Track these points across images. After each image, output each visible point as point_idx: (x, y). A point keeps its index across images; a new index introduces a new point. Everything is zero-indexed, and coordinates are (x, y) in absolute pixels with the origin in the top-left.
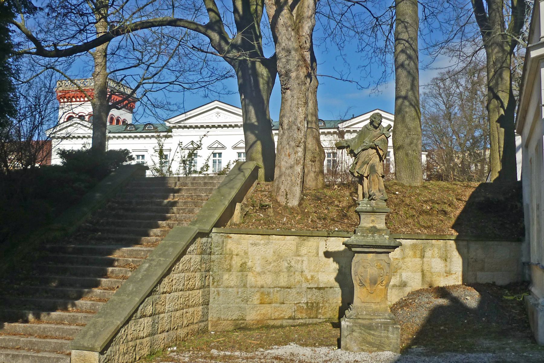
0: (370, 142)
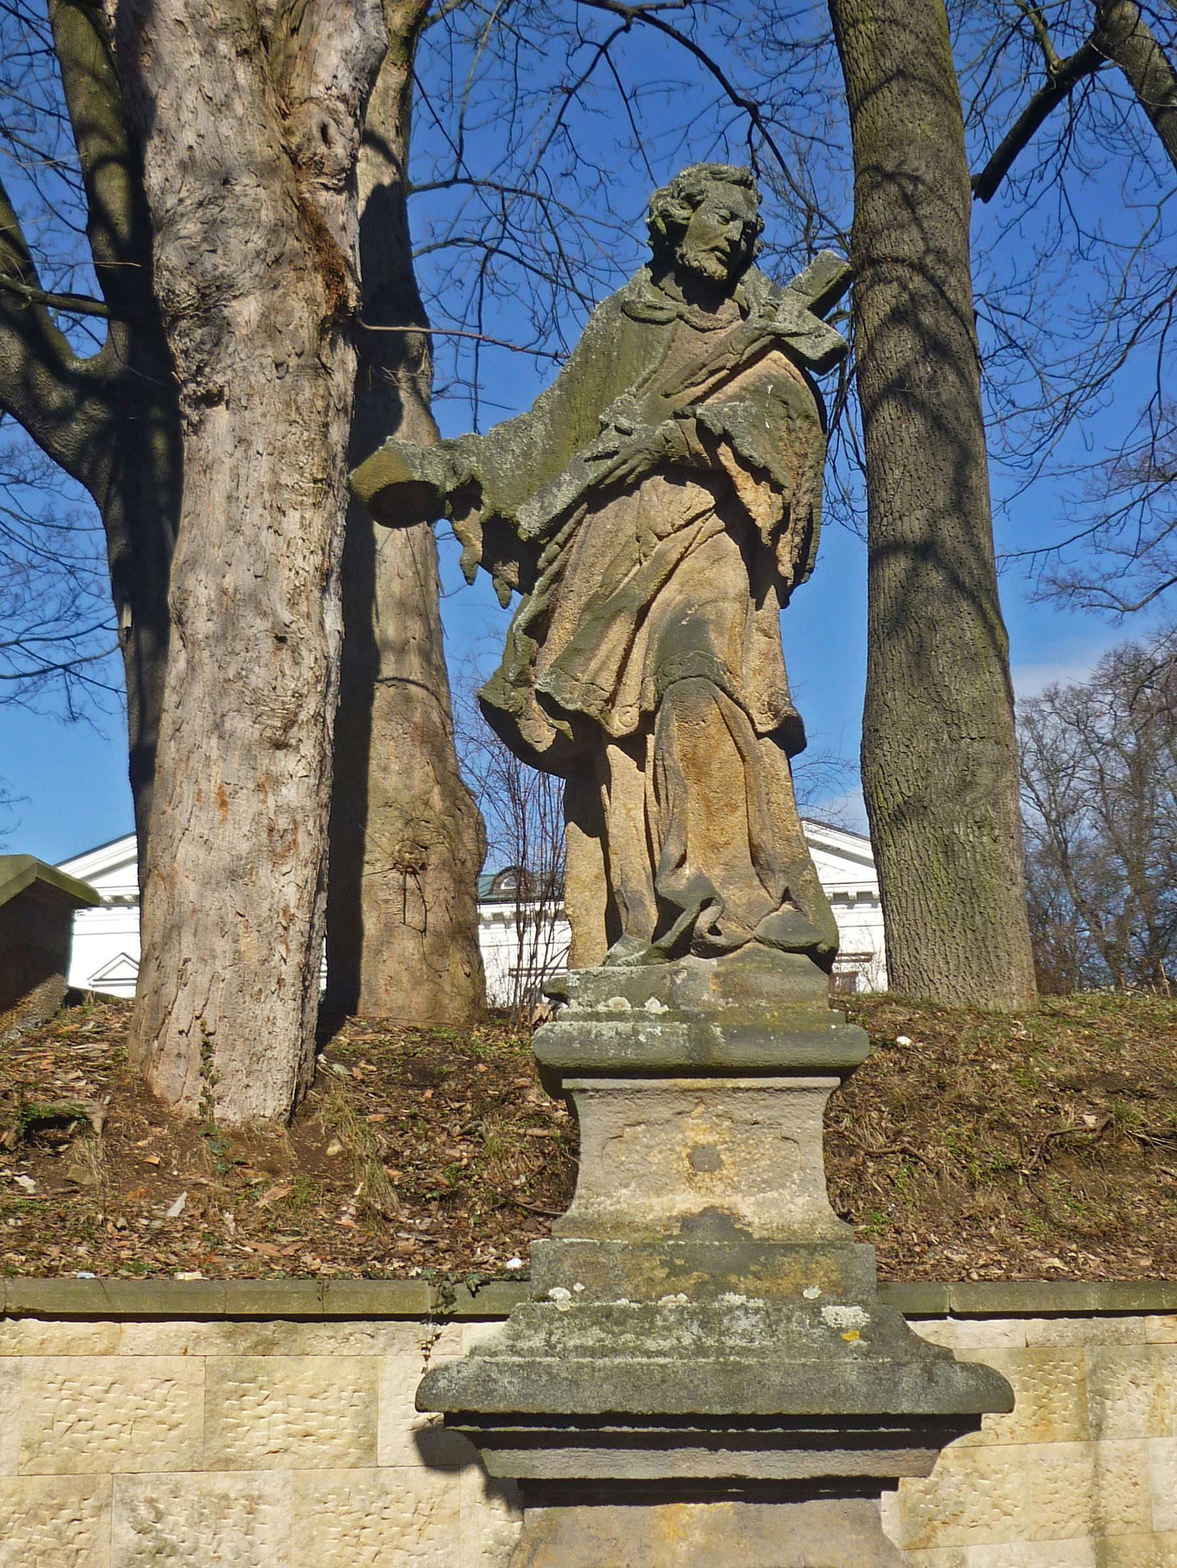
0: (653, 415)
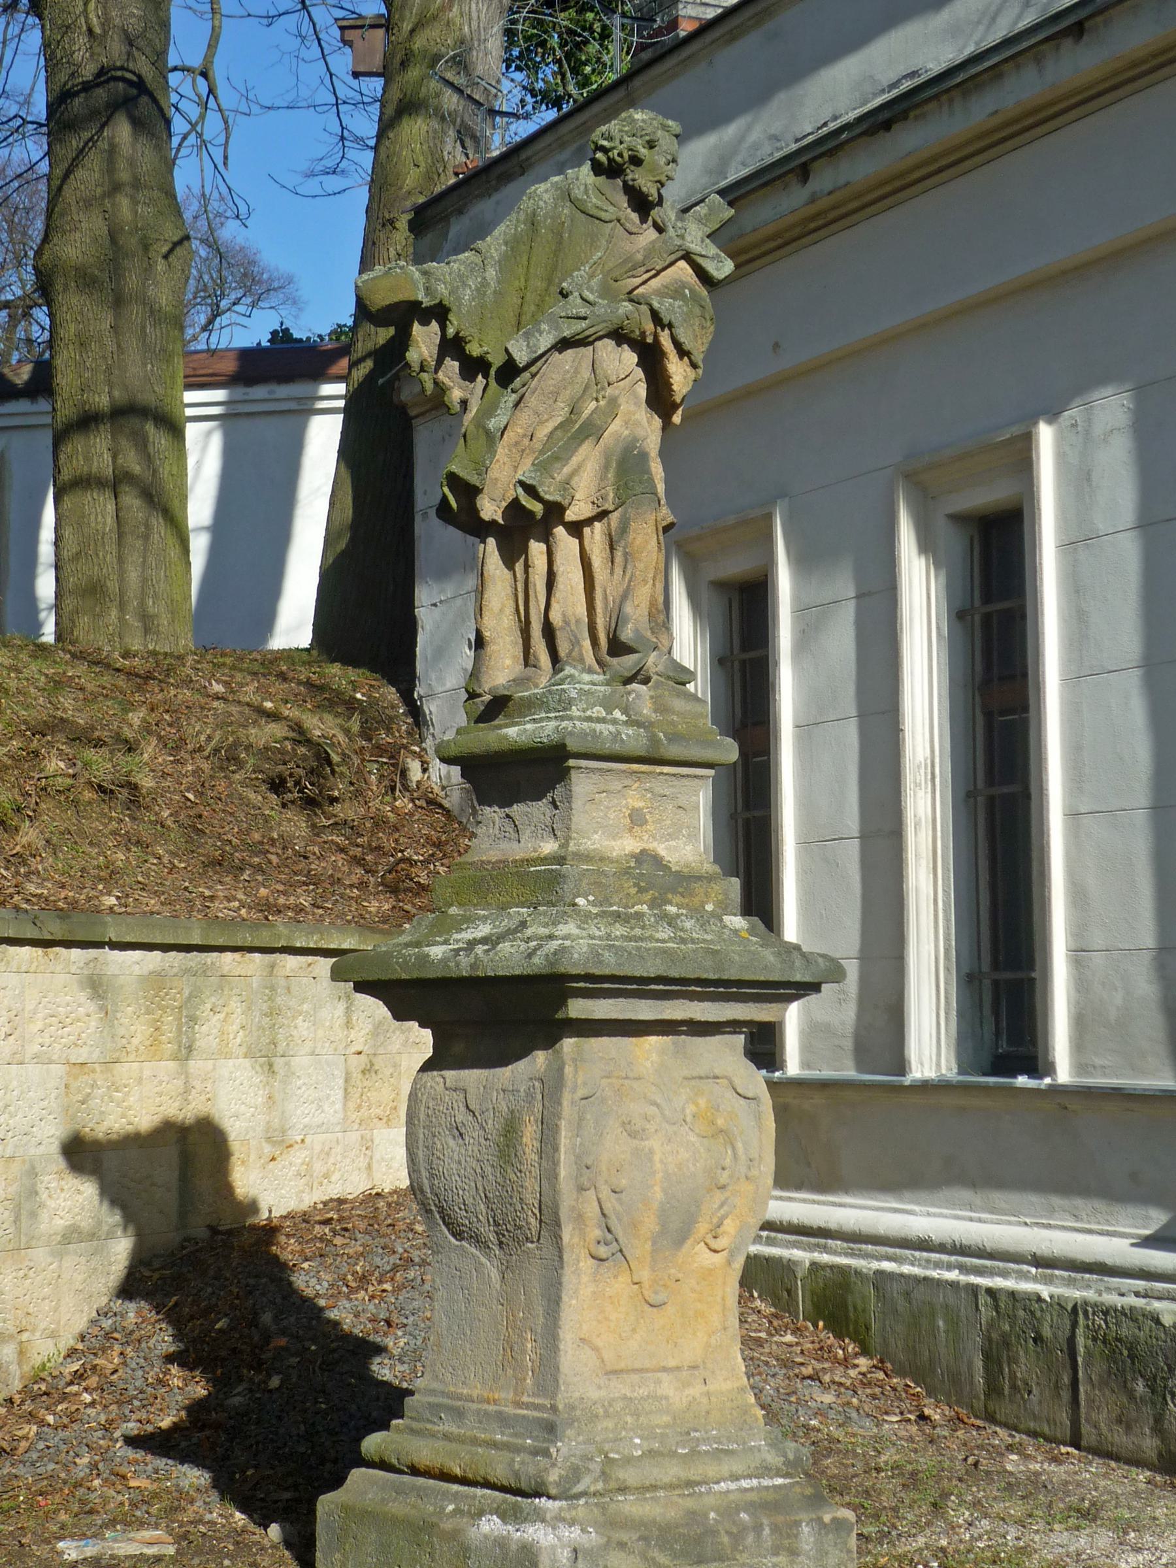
0: (606, 292)
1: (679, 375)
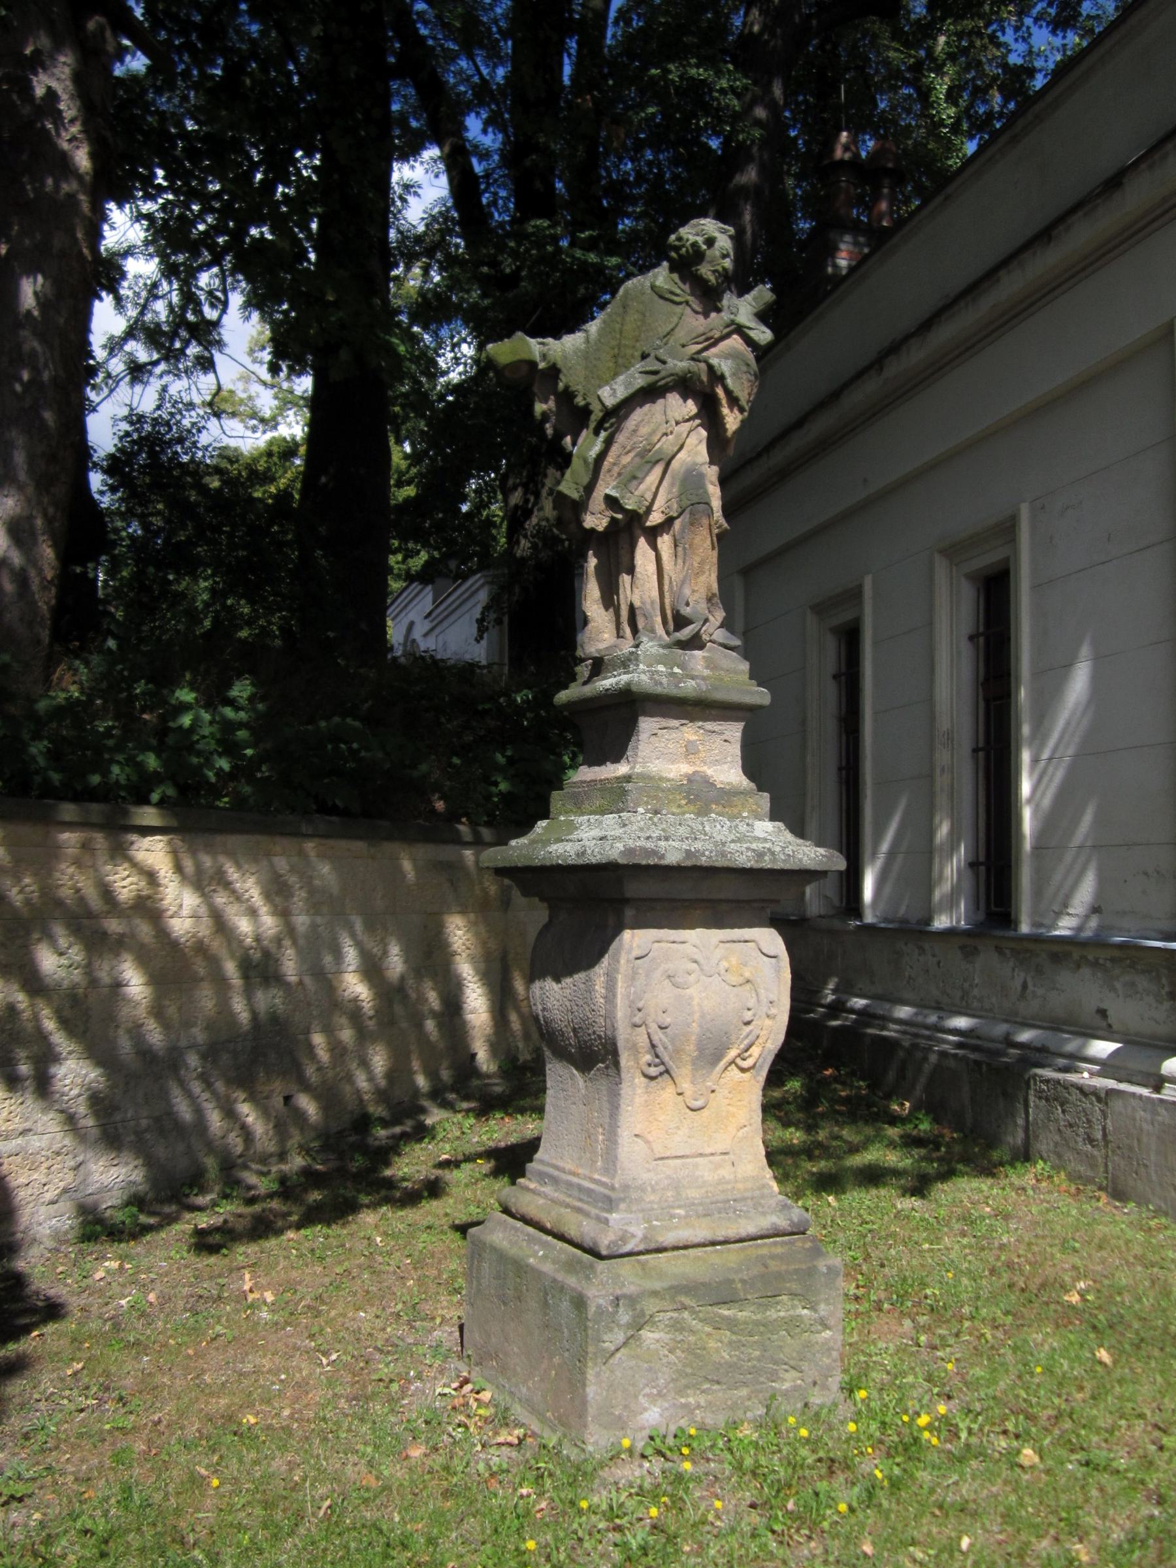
1: (732, 420)
